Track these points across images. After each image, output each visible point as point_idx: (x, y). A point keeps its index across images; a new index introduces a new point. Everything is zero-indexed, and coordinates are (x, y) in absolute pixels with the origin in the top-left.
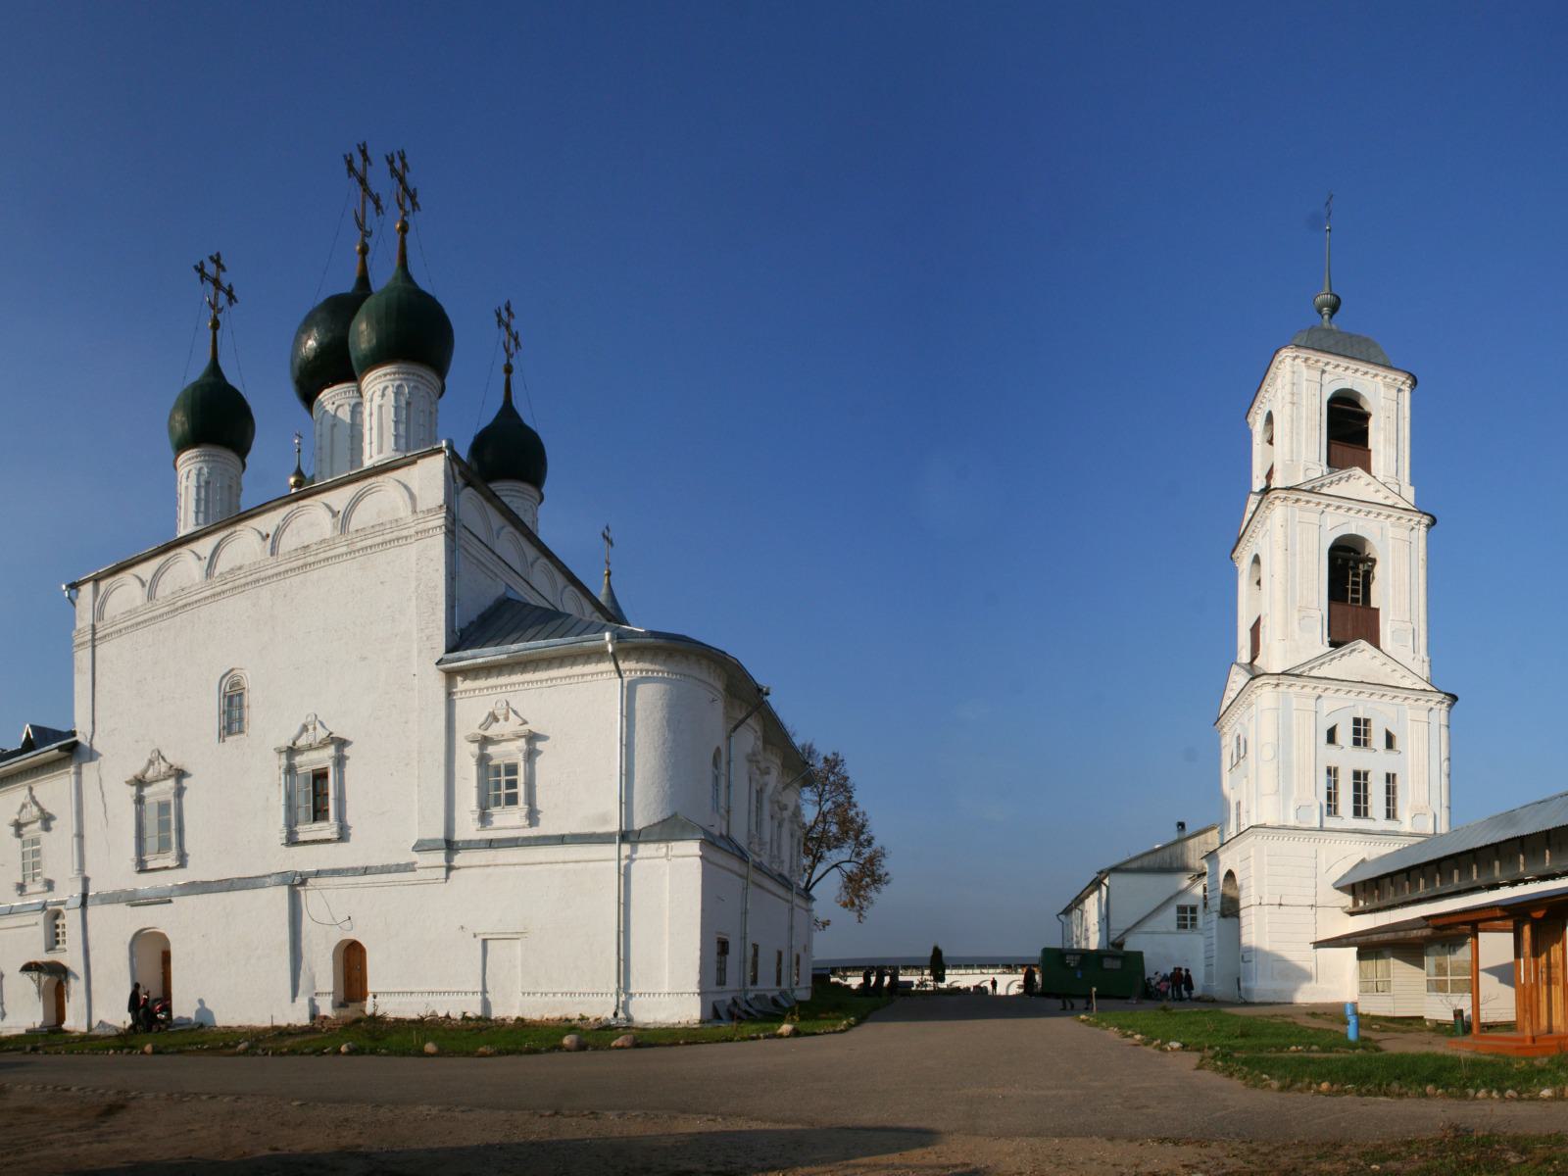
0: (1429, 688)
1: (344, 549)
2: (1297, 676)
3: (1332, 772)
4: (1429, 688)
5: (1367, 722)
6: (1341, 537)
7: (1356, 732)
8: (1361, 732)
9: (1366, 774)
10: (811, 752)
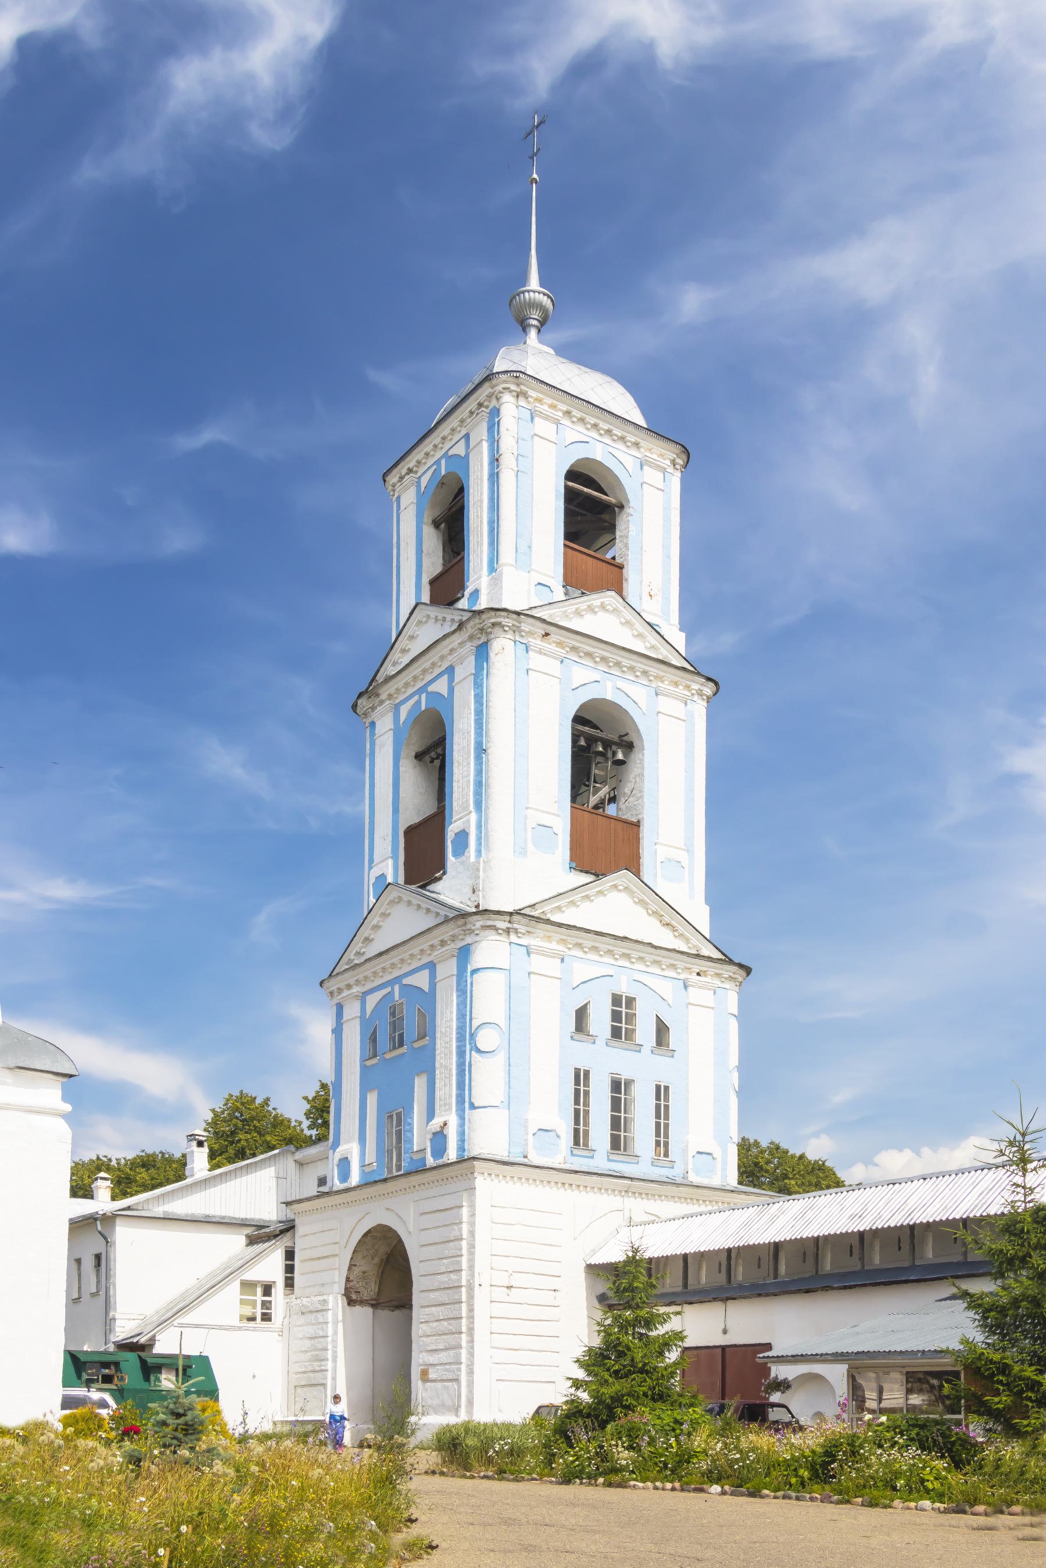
0: (708, 951)
1: (473, 817)
2: (538, 920)
3: (581, 1077)
4: (708, 951)
5: (631, 1001)
6: (593, 699)
7: (616, 1016)
9: (629, 1083)
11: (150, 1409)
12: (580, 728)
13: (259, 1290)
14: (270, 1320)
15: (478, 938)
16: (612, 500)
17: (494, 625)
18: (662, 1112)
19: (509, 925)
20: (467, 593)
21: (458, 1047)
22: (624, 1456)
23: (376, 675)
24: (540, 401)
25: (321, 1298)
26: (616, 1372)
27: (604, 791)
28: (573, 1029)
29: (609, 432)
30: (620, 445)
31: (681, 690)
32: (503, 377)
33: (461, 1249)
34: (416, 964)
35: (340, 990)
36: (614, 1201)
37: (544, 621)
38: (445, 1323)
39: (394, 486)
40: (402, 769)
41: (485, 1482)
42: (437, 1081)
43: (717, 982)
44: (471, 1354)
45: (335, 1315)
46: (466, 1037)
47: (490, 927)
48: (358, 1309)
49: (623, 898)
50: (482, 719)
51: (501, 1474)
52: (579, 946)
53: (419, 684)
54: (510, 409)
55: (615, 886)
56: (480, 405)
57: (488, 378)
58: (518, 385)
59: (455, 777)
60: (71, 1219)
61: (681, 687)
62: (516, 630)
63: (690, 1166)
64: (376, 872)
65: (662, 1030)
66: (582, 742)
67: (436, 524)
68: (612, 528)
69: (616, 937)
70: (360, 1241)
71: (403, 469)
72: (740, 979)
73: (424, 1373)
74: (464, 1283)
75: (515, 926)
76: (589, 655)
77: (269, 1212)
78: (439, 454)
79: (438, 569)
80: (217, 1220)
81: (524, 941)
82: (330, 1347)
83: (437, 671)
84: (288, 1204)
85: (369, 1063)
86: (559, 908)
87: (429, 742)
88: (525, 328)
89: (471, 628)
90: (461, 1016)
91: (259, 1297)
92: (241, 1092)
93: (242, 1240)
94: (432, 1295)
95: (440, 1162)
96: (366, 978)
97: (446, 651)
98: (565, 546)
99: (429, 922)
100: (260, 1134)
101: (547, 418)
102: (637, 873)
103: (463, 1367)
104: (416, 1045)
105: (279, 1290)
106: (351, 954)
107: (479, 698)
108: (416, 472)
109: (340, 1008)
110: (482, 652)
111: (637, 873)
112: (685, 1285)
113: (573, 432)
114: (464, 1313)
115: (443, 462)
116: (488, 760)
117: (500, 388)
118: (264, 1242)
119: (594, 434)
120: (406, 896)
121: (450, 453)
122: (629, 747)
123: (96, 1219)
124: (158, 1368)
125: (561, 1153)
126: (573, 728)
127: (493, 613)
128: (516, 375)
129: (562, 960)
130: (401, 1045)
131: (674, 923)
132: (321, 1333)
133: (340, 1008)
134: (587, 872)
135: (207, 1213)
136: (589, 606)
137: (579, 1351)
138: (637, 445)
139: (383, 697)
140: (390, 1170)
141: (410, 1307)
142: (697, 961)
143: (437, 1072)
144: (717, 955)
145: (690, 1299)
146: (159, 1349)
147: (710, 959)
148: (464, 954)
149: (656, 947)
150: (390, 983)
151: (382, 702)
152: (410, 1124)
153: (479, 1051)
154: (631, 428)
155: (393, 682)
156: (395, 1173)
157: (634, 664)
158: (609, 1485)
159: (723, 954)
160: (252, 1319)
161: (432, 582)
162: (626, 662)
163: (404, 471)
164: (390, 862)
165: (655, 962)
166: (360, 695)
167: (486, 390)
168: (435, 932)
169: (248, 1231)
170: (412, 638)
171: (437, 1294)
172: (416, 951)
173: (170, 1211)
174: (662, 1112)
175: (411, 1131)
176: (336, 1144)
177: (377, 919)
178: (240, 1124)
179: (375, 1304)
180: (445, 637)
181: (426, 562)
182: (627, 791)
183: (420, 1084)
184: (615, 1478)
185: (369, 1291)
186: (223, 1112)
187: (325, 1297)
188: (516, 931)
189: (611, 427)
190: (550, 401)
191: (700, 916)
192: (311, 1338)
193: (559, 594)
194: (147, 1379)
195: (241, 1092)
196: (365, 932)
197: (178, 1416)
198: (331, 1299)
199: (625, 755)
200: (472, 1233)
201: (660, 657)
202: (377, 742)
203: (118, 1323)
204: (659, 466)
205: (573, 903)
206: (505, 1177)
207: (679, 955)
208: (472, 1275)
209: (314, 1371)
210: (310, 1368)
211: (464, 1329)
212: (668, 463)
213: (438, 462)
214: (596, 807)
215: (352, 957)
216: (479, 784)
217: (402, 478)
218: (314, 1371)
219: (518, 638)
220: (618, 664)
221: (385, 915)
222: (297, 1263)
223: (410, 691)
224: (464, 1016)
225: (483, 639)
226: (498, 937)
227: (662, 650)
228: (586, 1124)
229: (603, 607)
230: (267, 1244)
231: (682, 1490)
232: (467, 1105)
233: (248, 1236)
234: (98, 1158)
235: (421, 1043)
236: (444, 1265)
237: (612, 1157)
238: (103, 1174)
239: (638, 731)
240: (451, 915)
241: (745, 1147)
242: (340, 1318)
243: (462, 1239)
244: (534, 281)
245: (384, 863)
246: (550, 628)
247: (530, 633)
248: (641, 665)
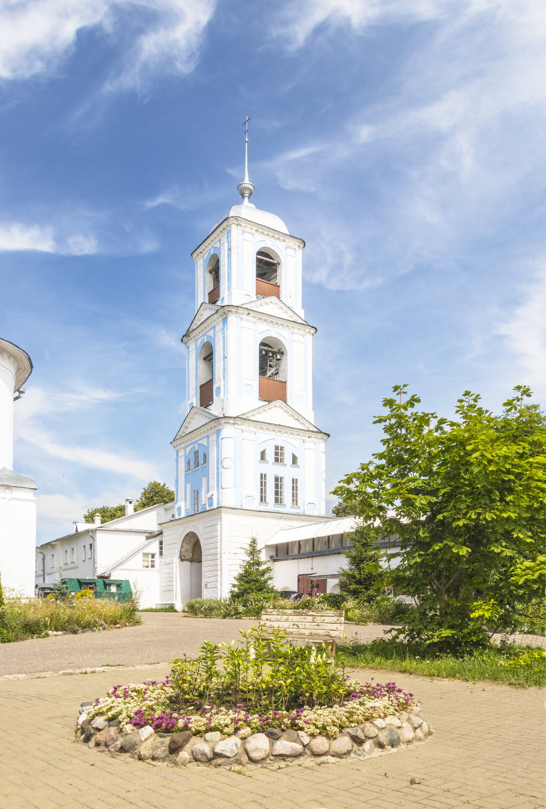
0: (312, 429)
1: (222, 382)
2: (245, 419)
3: (263, 477)
5: (282, 448)
7: (277, 454)
8: (279, 453)
9: (281, 478)
10: (401, 502)
12: (263, 347)
13: (150, 556)
14: (154, 567)
15: (223, 427)
16: (275, 262)
17: (228, 311)
18: (295, 488)
19: (235, 422)
20: (220, 299)
21: (217, 467)
22: (241, 609)
23: (189, 329)
24: (246, 227)
25: (171, 559)
26: (247, 581)
27: (273, 370)
28: (260, 459)
29: (273, 236)
30: (278, 241)
31: (302, 332)
32: (231, 219)
33: (217, 540)
34: (202, 436)
35: (177, 446)
36: (276, 522)
37: (247, 309)
38: (213, 567)
39: (195, 258)
40: (198, 364)
41: (201, 619)
42: (210, 479)
43: (316, 440)
44: (221, 578)
45: (176, 565)
46: (219, 463)
47: (227, 423)
48: (185, 562)
49: (279, 410)
50: (225, 346)
51: (206, 616)
52: (262, 428)
53: (204, 333)
54: (234, 229)
55: (276, 406)
56: (224, 229)
57: (226, 219)
58: (237, 221)
59: (216, 367)
61: (302, 331)
62: (237, 313)
63: (306, 508)
64: (190, 402)
65: (294, 459)
66: (264, 353)
67: (211, 272)
68: (276, 271)
69: (275, 425)
70: (184, 538)
71: (198, 252)
72: (325, 439)
73: (206, 585)
74: (219, 552)
75: (237, 422)
76: (265, 320)
77: (155, 528)
78: (210, 246)
79: (212, 288)
80: (135, 531)
81: (241, 427)
82: (174, 576)
83: (210, 328)
84: (160, 524)
85: (187, 472)
86: (254, 415)
87: (208, 353)
88: (243, 197)
89: (221, 312)
90: (218, 455)
91: (150, 559)
92: (155, 481)
93: (144, 538)
94: (208, 557)
95: (211, 508)
96: (186, 441)
97: (212, 321)
98: (256, 280)
99: (207, 420)
100: (162, 498)
101: (249, 233)
102: (285, 402)
103: (219, 583)
104: (203, 466)
105: (157, 556)
106: (181, 433)
107: (224, 338)
108: (203, 253)
109: (177, 452)
110: (225, 320)
111: (285, 402)
112: (299, 552)
113: (259, 237)
114: (219, 563)
115: (212, 250)
116: (227, 361)
117: (230, 223)
118: (151, 538)
119: (267, 238)
120: (199, 411)
121: (214, 246)
122: (282, 353)
123: (89, 531)
124: (110, 585)
125: (256, 504)
126: (259, 347)
127: (228, 307)
128: (236, 218)
129: (255, 434)
130: (198, 466)
131: (299, 419)
132: (172, 572)
133: (177, 452)
134: (265, 401)
135: (131, 528)
136: (265, 302)
137: (236, 574)
138: (284, 240)
139: (192, 337)
140: (195, 511)
141: (201, 561)
142: (308, 432)
143: (210, 476)
144: (316, 430)
145: (301, 557)
146: (112, 578)
147: (313, 431)
148: (218, 432)
149: (291, 428)
150: (194, 443)
151: (191, 339)
152: (201, 495)
153: (224, 468)
154: (282, 235)
155: (194, 332)
156: (196, 513)
157: (283, 323)
158: (236, 618)
159: (318, 429)
160: (147, 567)
161: (209, 294)
162: (280, 322)
163: (199, 253)
164: (195, 398)
165: (291, 433)
166: (184, 336)
167: (225, 224)
168: (209, 424)
169: (147, 534)
170: (201, 315)
171: (210, 556)
172: (202, 431)
173: (117, 528)
174: (295, 488)
175: (202, 497)
176: (177, 502)
177: (189, 419)
178: (154, 494)
179: (191, 561)
180: (212, 315)
181: (207, 286)
182: (282, 370)
183: (204, 480)
184: (238, 616)
185: (189, 555)
186: (148, 489)
187: (173, 558)
188: (237, 424)
189: (274, 235)
190: (250, 227)
191: (310, 416)
192: (168, 573)
193: (254, 298)
194: (105, 588)
195: (155, 481)
196: (186, 424)
197: (59, 590)
198: (174, 559)
199: (281, 357)
200: (221, 534)
201: (294, 320)
202: (190, 353)
203: (98, 569)
204: (292, 248)
205: (259, 413)
206: (233, 514)
207: (301, 431)
208: (221, 550)
209: (169, 586)
210: (168, 584)
211: (219, 569)
212: (297, 246)
213: (210, 249)
214: (270, 377)
215: (181, 433)
216: (224, 370)
217: (198, 255)
218: (169, 586)
219: (238, 316)
220: (277, 323)
221: (192, 418)
222: (163, 546)
223: (201, 335)
224: (218, 455)
225: (225, 316)
226: (230, 426)
227: (294, 317)
228: (265, 493)
229: (271, 302)
230: (153, 539)
231: (257, 619)
232: (220, 488)
233: (146, 537)
234: (104, 507)
235: (205, 465)
236: (212, 546)
237: (275, 505)
238: (97, 514)
239: (285, 348)
240: (214, 418)
242: (178, 566)
243: (217, 537)
244: (247, 180)
245: (192, 399)
246: (250, 312)
247: (242, 314)
248: (285, 323)
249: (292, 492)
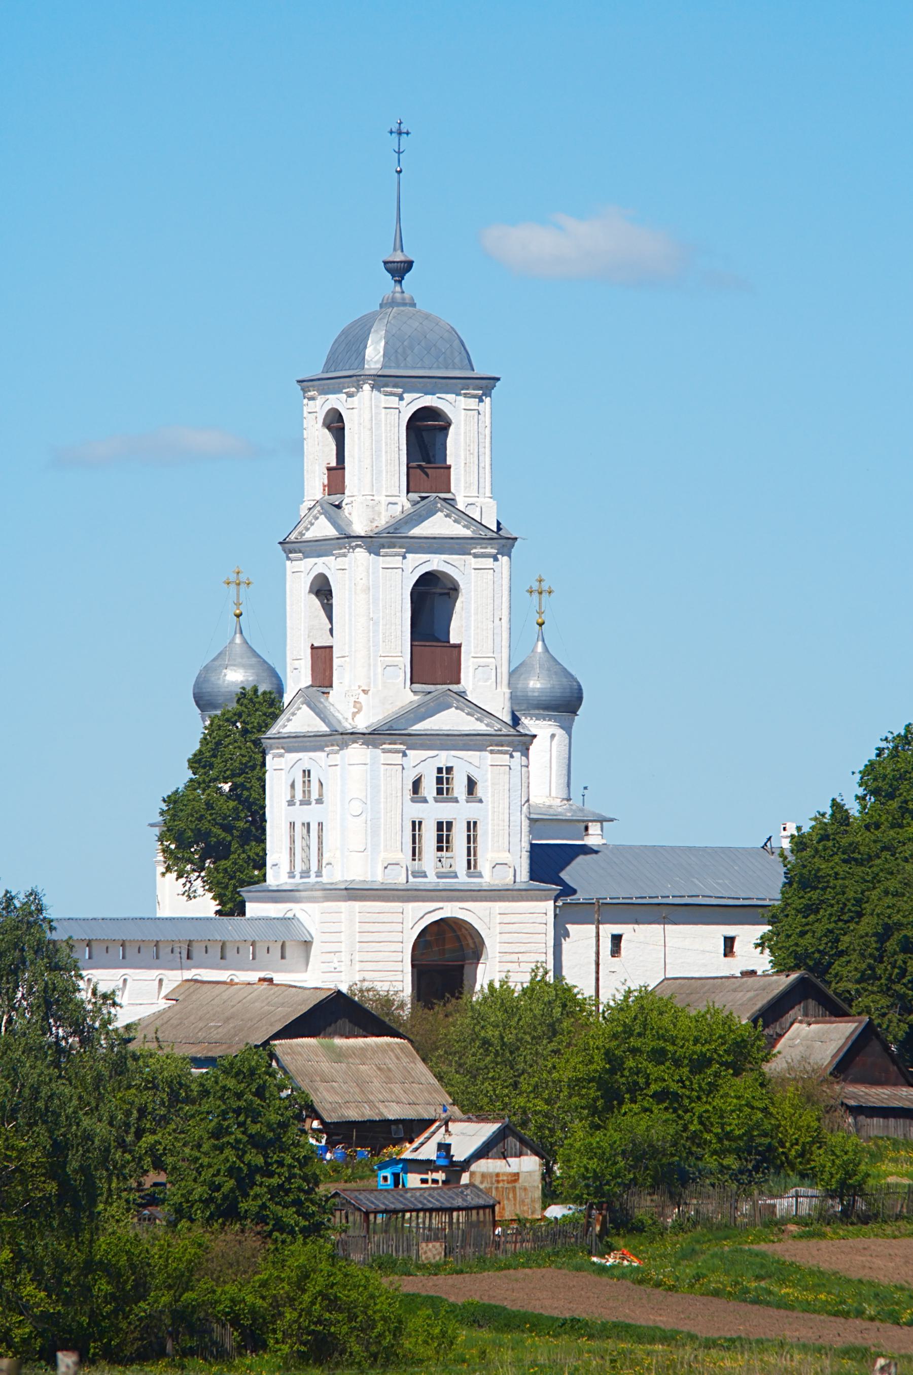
3: (416, 826)
7: (439, 781)
8: (444, 777)
11: (101, 1259)
18: (471, 839)
60: (311, 591)
65: (471, 785)
174: (471, 839)
241: (535, 850)
249: (466, 833)
